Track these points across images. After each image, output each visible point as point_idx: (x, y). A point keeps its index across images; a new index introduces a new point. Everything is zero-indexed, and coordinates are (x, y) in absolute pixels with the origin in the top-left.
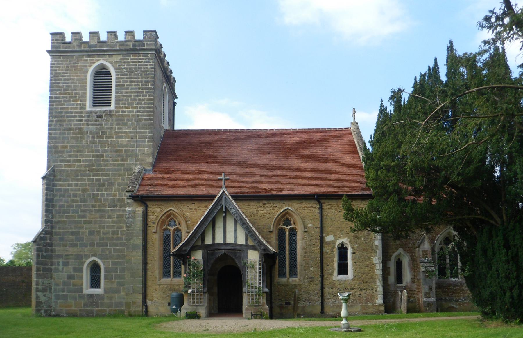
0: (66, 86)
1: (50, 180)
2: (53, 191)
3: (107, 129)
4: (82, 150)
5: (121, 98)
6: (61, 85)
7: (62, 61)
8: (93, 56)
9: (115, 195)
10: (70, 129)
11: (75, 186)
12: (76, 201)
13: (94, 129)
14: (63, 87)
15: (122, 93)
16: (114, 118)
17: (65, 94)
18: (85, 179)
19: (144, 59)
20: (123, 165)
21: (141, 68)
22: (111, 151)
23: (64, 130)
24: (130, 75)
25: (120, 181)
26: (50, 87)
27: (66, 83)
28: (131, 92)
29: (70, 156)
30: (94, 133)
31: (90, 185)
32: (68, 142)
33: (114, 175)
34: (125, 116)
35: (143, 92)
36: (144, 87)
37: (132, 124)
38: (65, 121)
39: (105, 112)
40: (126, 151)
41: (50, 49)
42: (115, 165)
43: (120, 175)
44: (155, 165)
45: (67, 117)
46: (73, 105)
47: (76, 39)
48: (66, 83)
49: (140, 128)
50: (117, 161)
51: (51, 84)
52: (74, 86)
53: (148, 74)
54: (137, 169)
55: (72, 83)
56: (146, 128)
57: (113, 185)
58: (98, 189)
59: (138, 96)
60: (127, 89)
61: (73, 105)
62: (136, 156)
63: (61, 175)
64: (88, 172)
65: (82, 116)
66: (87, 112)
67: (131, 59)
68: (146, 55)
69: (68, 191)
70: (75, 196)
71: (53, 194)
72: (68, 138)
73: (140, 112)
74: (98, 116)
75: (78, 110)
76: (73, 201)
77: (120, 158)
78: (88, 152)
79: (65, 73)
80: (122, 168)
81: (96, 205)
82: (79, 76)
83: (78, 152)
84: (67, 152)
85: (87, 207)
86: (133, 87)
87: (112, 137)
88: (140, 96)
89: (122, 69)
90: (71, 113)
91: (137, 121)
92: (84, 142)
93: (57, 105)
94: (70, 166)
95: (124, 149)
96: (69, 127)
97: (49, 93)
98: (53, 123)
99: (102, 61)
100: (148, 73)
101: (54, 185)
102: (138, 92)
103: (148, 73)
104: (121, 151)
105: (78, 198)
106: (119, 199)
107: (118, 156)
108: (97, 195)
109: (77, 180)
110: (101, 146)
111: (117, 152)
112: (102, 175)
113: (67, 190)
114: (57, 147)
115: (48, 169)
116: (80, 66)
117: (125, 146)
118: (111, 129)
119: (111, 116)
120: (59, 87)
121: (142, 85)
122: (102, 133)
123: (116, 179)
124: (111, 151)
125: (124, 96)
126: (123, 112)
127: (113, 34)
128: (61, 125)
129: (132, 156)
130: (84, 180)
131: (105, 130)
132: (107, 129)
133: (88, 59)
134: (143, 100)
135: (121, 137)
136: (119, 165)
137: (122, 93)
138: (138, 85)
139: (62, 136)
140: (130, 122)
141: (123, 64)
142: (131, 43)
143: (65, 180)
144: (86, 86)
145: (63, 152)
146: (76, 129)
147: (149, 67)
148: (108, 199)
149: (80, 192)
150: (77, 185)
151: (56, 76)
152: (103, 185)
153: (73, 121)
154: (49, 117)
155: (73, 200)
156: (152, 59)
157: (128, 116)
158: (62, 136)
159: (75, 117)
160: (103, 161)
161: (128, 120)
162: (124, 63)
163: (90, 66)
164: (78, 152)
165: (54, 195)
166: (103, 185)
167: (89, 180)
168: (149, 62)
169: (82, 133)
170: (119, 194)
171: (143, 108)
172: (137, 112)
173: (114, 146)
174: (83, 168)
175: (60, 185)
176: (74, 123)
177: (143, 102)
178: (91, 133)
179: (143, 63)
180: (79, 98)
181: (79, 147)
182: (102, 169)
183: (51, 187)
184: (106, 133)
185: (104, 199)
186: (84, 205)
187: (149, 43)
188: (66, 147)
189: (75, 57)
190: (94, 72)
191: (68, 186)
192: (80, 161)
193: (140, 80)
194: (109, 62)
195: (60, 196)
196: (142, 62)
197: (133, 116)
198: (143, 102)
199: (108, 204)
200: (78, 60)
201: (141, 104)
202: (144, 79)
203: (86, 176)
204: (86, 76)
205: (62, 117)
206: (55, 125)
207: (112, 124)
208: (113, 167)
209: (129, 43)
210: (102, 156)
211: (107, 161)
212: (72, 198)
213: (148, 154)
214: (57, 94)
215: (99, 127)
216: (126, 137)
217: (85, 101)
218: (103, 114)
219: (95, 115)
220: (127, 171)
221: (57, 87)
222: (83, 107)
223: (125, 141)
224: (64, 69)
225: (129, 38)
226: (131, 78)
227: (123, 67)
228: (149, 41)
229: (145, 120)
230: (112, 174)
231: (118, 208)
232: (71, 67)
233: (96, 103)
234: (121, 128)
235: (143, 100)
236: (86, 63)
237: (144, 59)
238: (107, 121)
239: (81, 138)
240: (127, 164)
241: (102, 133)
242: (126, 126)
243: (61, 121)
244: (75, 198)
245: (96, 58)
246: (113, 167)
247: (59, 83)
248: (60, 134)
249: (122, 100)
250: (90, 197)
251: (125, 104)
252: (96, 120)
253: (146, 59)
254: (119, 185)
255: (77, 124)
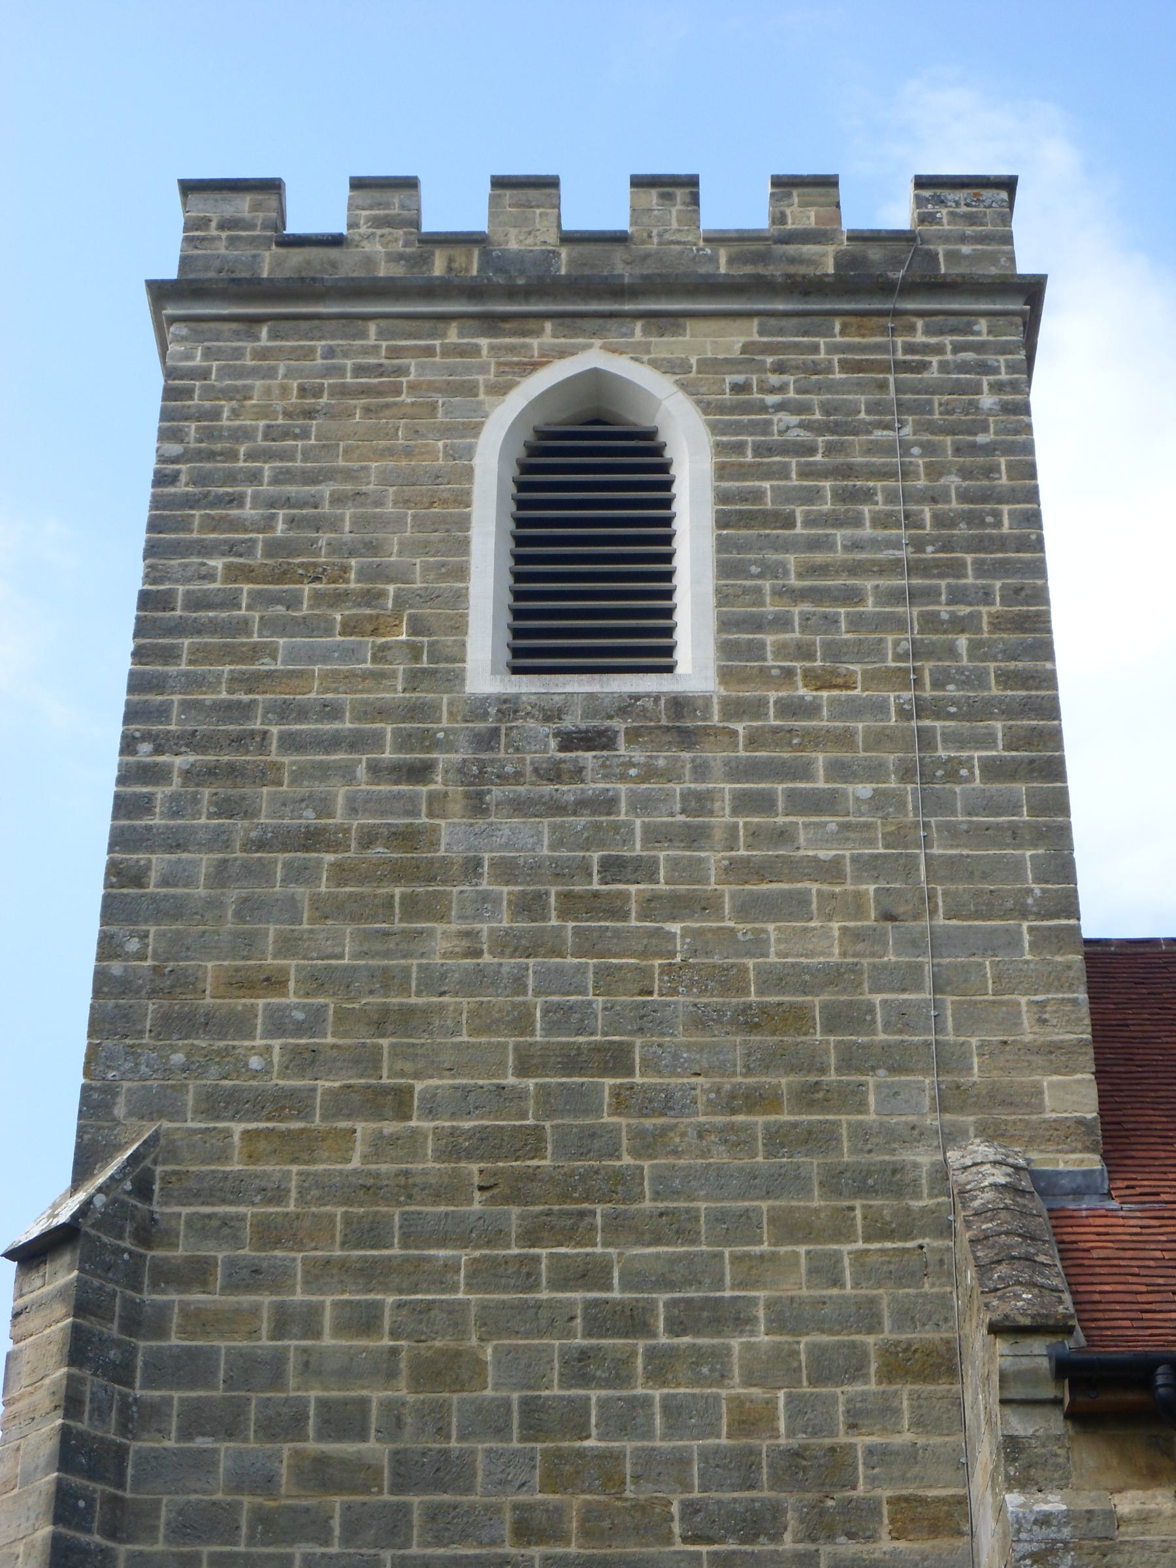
0: (291, 521)
1: (102, 1255)
2: (122, 1373)
3: (654, 836)
4: (426, 1012)
5: (770, 608)
6: (248, 512)
7: (262, 354)
8: (527, 322)
9: (750, 1420)
10: (313, 839)
11: (341, 1328)
12: (357, 1476)
13: (536, 839)
14: (268, 524)
15: (774, 571)
16: (716, 756)
17: (282, 575)
18: (452, 1267)
19: (939, 350)
20: (818, 1139)
21: (921, 408)
22: (700, 1021)
23: (261, 845)
24: (830, 449)
25: (798, 1287)
26: (154, 525)
27: (288, 502)
28: (854, 569)
29: (305, 1060)
30: (534, 870)
31: (493, 1322)
32: (288, 945)
33: (740, 1226)
34: (815, 739)
35: (956, 569)
36: (962, 530)
37: (879, 802)
38: (267, 775)
39: (628, 706)
40: (835, 1020)
41: (170, 272)
42: (736, 1139)
43: (791, 1228)
44: (1116, 1134)
45: (291, 743)
46: (349, 653)
47: (378, 222)
48: (288, 502)
49: (952, 833)
50: (755, 1100)
51: (157, 502)
52: (360, 523)
53: (989, 449)
54: (981, 1165)
55: (338, 500)
56: (1015, 835)
57: (735, 1317)
58: (584, 1355)
59: (915, 595)
60: (814, 545)
61: (349, 653)
62: (946, 1060)
63: (201, 1228)
64: (477, 1204)
65: (427, 740)
66: (478, 708)
67: (833, 349)
68: (962, 322)
69: (277, 1379)
70: (345, 1420)
71: (125, 1406)
72: (291, 909)
73: (939, 713)
74: (569, 741)
75: (396, 692)
76: (320, 1474)
77: (784, 1081)
78: (483, 1022)
79: (286, 434)
80: (812, 1164)
81: (558, 1512)
82: (408, 453)
83: (381, 1022)
84: (278, 1025)
85: (464, 1537)
86: (867, 531)
87: (708, 906)
88: (931, 594)
89: (763, 408)
90: (331, 711)
91: (927, 777)
92: (441, 945)
93: (201, 655)
94: (300, 1146)
95: (816, 1001)
96: (309, 817)
97: (138, 568)
98: (161, 792)
99: (594, 357)
100: (981, 439)
101: (136, 1321)
102: (917, 568)
103: (981, 439)
104: (798, 1018)
105: (375, 1449)
106: (797, 1454)
107: (769, 1061)
108: (574, 1420)
109: (372, 1274)
110: (607, 979)
111: (753, 1027)
112: (618, 1227)
113: (265, 1370)
114: (186, 983)
115: (82, 1169)
116: (412, 387)
117: (834, 976)
118: (695, 836)
119: (687, 738)
120: (236, 525)
121: (940, 521)
122: (613, 868)
123: (752, 1270)
124: (700, 1021)
125: (798, 595)
126: (789, 708)
127: (680, 194)
128: (226, 808)
129: (897, 1061)
130: (442, 1276)
131: (638, 850)
132: (654, 836)
133: (484, 342)
134: (959, 625)
135: (797, 905)
136: (777, 1139)
137: (774, 571)
138: (912, 520)
139: (233, 895)
140: (864, 790)
141: (774, 379)
142: (831, 249)
143: (252, 1277)
144: (464, 523)
145: (241, 1025)
146: (368, 838)
147: (987, 400)
148: (681, 1461)
149: (402, 1391)
150: (364, 1320)
151: (211, 456)
152: (634, 1321)
153: (347, 772)
154: (128, 745)
155: (322, 1461)
156: (1004, 349)
157: (844, 739)
158: (233, 895)
159: (356, 742)
160: (622, 1101)
161: (839, 770)
162: (780, 368)
163: (501, 390)
164: (381, 1022)
165: (134, 1418)
166: (634, 1321)
167: (485, 1274)
168: (985, 368)
169: (429, 872)
170: (797, 1406)
171: (963, 684)
172: (921, 709)
173: (730, 980)
174: (429, 1165)
175: (198, 1321)
176: (349, 797)
177: (962, 642)
178: (506, 870)
179: (933, 374)
180: (401, 601)
181: (388, 980)
182: (619, 1177)
183: (113, 1330)
184: (645, 870)
185: (647, 1458)
186: (433, 1514)
187: (966, 249)
188: (274, 983)
189: (372, 328)
190: (528, 435)
191: (280, 1330)
192: (398, 1102)
193: (922, 483)
194: (655, 364)
195: (195, 1421)
196: (923, 366)
197: (878, 739)
198: (962, 642)
199: (691, 1509)
200: (394, 352)
201: (951, 651)
202: (953, 481)
203: (464, 1241)
204: (469, 452)
205: (239, 741)
206: (176, 807)
207: (699, 803)
208: (720, 1157)
209: (808, 249)
210: (616, 1059)
211: (667, 1103)
212: (312, 1446)
213: (1052, 1049)
214: (210, 577)
215: (581, 821)
216: (831, 907)
217: (459, 626)
218: (619, 725)
219: (545, 729)
220: (863, 1190)
221: (214, 524)
222: (443, 667)
223: (826, 941)
224: (279, 405)
225: (804, 215)
226: (848, 471)
227: (771, 399)
228: (963, 239)
229: (993, 770)
230: (719, 1217)
231: (788, 1543)
232: (343, 391)
233: (534, 644)
234: (783, 836)
235: (959, 625)
236: (468, 370)
237: (939, 350)
238: (649, 773)
239: (413, 907)
240: (861, 1133)
241: (613, 868)
242: (832, 823)
243: (233, 772)
244: (348, 1448)
245: (548, 336)
246: (720, 1157)
247: (236, 500)
248: (221, 875)
249: (782, 623)
250: (501, 1432)
251: (804, 652)
252: (554, 773)
253: (958, 348)
254: (785, 1318)
255: (369, 798)
